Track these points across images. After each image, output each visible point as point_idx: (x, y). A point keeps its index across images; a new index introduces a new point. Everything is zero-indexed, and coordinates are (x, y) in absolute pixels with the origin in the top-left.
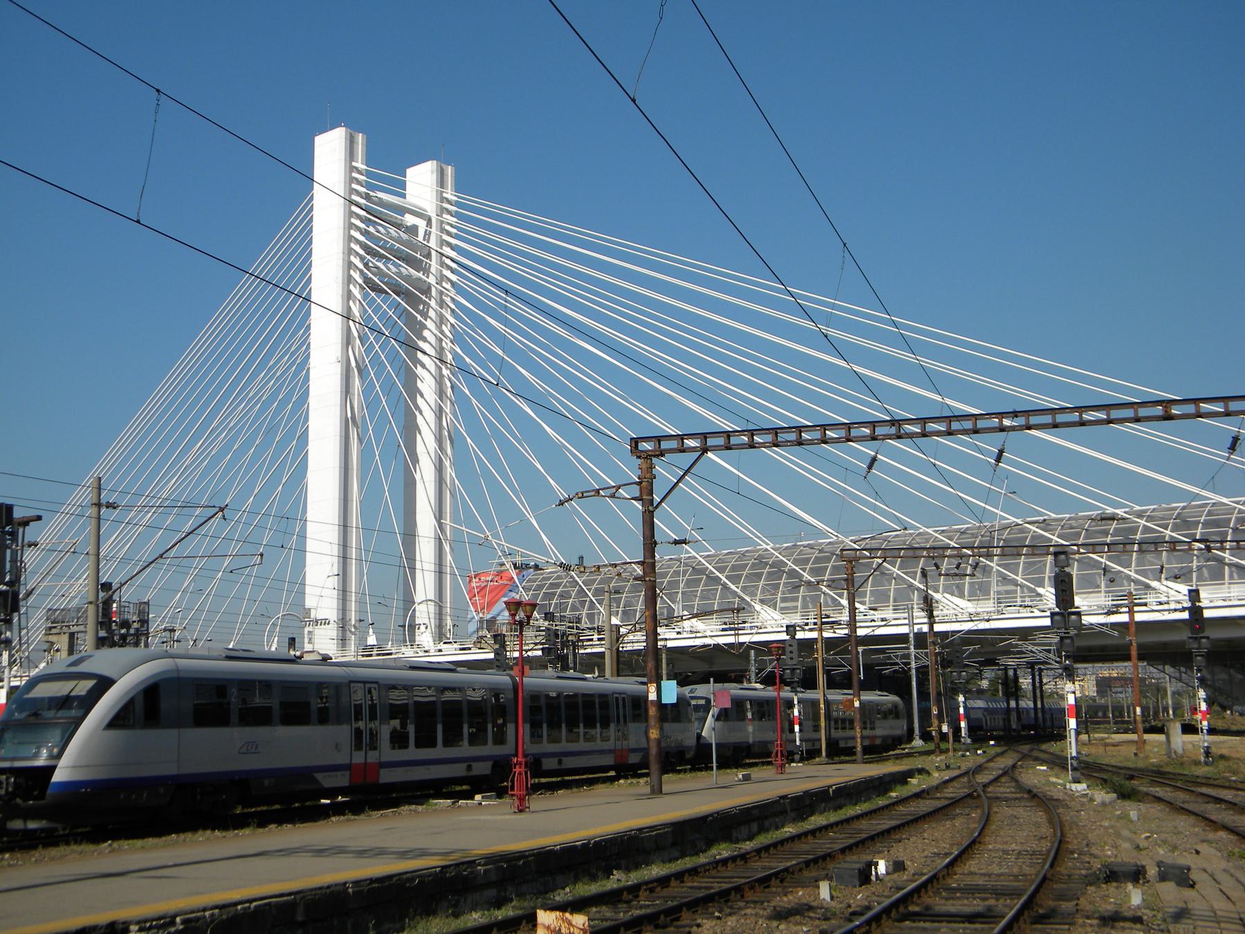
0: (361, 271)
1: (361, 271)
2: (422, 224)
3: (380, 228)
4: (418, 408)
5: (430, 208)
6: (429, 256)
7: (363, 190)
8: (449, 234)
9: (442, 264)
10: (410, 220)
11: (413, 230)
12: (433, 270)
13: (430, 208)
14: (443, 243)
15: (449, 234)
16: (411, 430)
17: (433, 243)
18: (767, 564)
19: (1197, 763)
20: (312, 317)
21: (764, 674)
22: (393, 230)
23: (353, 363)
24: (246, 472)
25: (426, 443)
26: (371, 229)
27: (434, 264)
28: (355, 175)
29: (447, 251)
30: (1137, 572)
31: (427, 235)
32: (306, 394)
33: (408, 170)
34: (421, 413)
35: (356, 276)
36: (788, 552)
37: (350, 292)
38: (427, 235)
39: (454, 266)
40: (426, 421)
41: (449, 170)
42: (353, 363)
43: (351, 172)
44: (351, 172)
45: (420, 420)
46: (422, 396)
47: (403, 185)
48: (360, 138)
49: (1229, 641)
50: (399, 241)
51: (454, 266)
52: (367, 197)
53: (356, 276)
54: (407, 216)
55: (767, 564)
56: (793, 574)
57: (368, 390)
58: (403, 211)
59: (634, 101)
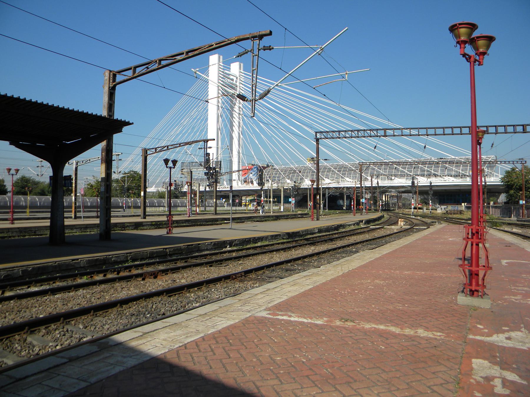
0: (221, 91)
1: (221, 91)
2: (235, 79)
3: (226, 80)
4: (234, 121)
5: (238, 75)
6: (237, 87)
7: (222, 70)
8: (242, 81)
9: (240, 89)
10: (231, 77)
11: (232, 80)
12: (238, 90)
13: (238, 75)
14: (240, 83)
15: (242, 81)
16: (232, 126)
17: (238, 84)
18: (327, 168)
19: (428, 214)
20: (208, 121)
21: (329, 195)
22: (228, 80)
23: (220, 115)
24: (202, 127)
25: (236, 129)
26: (224, 80)
27: (238, 88)
28: (220, 66)
29: (241, 85)
30: (407, 171)
31: (236, 81)
32: (207, 119)
33: (231, 64)
34: (234, 122)
35: (220, 92)
36: (332, 166)
37: (219, 92)
38: (236, 81)
39: (243, 89)
40: (236, 124)
41: (242, 64)
42: (220, 115)
43: (219, 77)
44: (219, 77)
45: (234, 124)
46: (235, 118)
47: (230, 69)
48: (221, 57)
49: (446, 190)
50: (230, 83)
51: (243, 89)
52: (223, 72)
53: (220, 92)
54: (231, 76)
55: (327, 168)
56: (333, 171)
57: (223, 120)
58: (229, 75)
59: (164, 88)
